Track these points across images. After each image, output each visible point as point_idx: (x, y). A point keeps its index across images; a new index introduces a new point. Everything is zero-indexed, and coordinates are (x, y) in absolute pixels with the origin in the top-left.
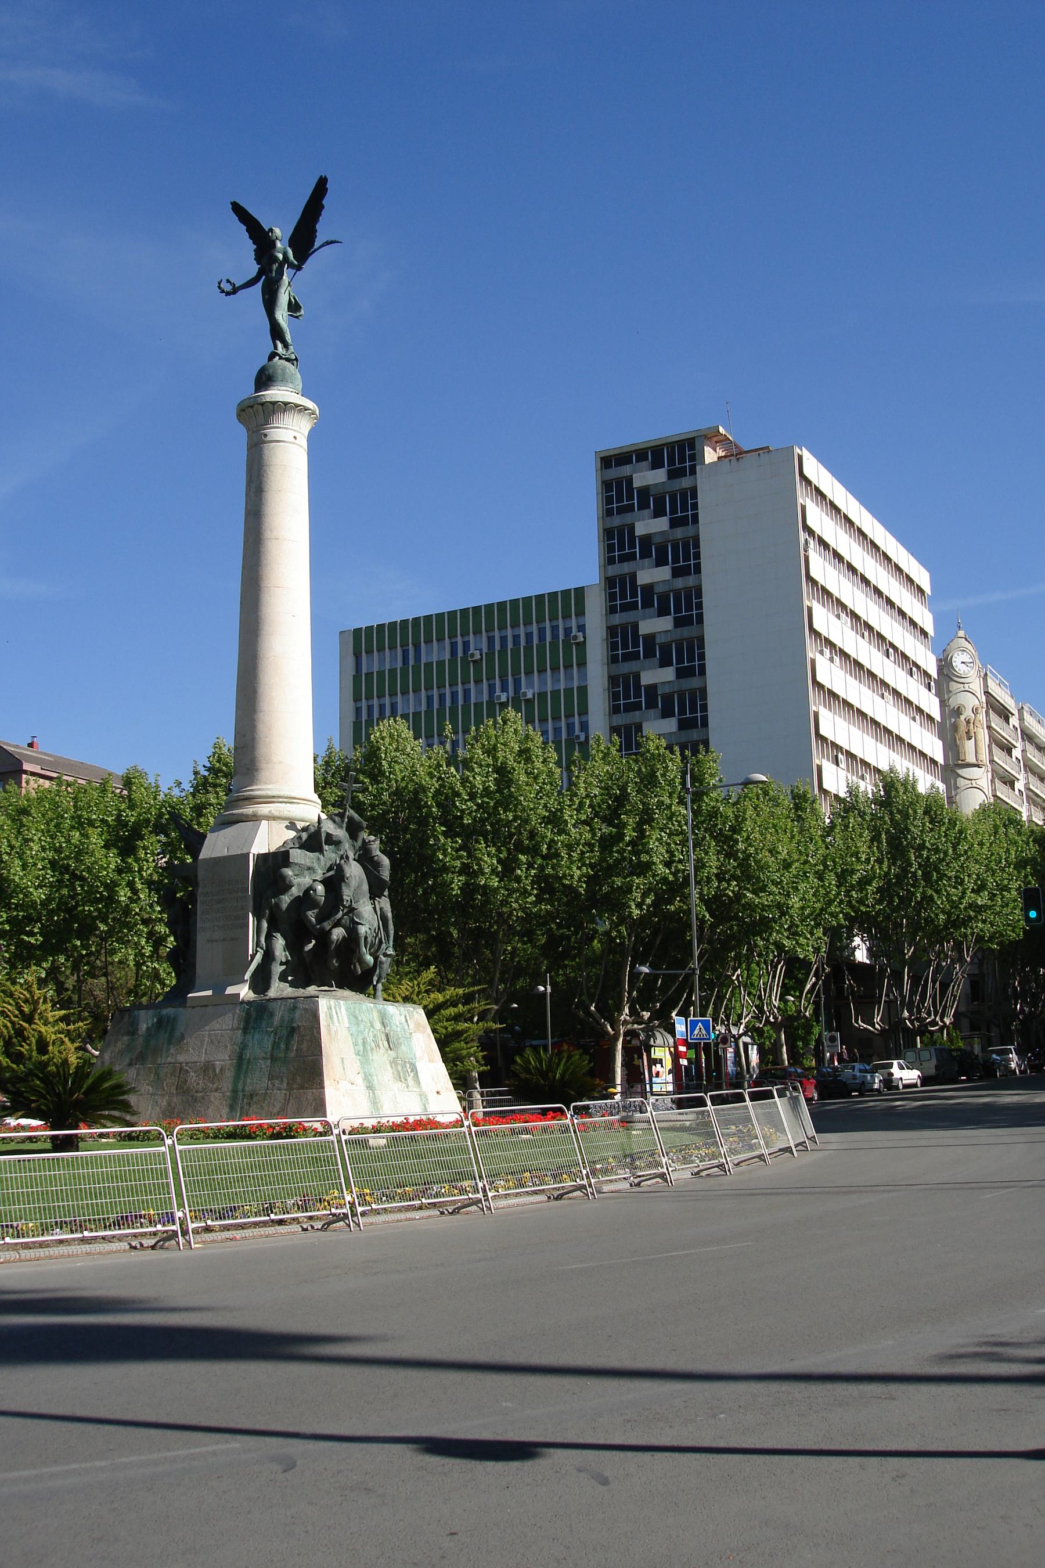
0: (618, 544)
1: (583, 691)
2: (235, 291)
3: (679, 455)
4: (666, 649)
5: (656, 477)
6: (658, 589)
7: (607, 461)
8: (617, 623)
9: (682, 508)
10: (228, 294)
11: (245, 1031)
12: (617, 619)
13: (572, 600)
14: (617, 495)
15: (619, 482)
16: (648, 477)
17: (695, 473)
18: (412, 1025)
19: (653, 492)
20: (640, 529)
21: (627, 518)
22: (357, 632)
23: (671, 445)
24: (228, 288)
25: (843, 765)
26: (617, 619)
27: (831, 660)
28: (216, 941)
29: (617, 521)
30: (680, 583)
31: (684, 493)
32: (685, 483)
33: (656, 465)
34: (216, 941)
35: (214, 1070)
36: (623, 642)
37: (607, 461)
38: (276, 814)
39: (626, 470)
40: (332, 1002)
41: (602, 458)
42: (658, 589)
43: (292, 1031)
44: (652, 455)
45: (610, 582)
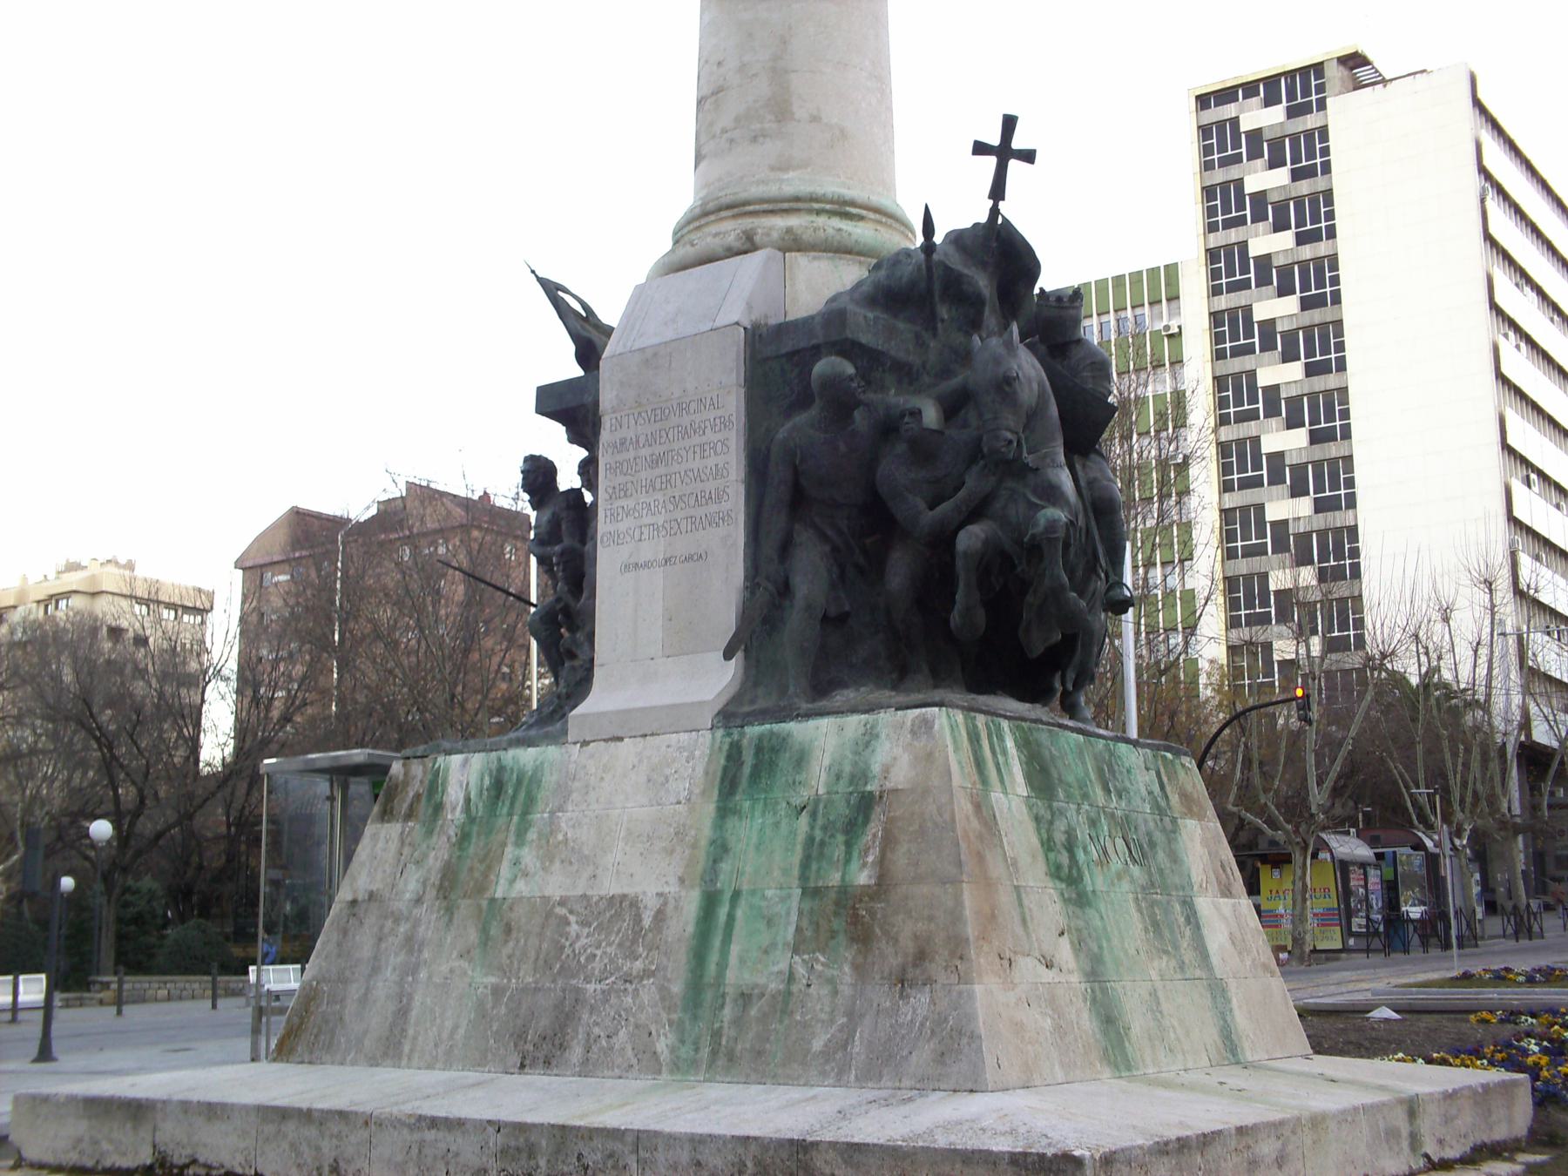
0: (1224, 204)
1: (1179, 398)
3: (1300, 87)
4: (1290, 337)
5: (1273, 117)
6: (1278, 261)
7: (1203, 101)
8: (1224, 307)
9: (1308, 154)
11: (725, 811)
13: (1162, 285)
14: (1220, 141)
15: (1221, 125)
16: (1257, 117)
18: (1175, 799)
19: (1267, 135)
20: (1251, 186)
21: (1234, 172)
23: (1290, 74)
25: (1536, 488)
26: (1223, 302)
27: (1518, 347)
28: (646, 565)
30: (1307, 252)
31: (1309, 134)
32: (1311, 121)
33: (1270, 101)
34: (646, 565)
35: (638, 919)
36: (1231, 330)
37: (1203, 101)
38: (807, 236)
39: (1229, 111)
40: (981, 720)
41: (1198, 97)
42: (1278, 261)
43: (865, 804)
44: (1268, 88)
45: (1212, 255)
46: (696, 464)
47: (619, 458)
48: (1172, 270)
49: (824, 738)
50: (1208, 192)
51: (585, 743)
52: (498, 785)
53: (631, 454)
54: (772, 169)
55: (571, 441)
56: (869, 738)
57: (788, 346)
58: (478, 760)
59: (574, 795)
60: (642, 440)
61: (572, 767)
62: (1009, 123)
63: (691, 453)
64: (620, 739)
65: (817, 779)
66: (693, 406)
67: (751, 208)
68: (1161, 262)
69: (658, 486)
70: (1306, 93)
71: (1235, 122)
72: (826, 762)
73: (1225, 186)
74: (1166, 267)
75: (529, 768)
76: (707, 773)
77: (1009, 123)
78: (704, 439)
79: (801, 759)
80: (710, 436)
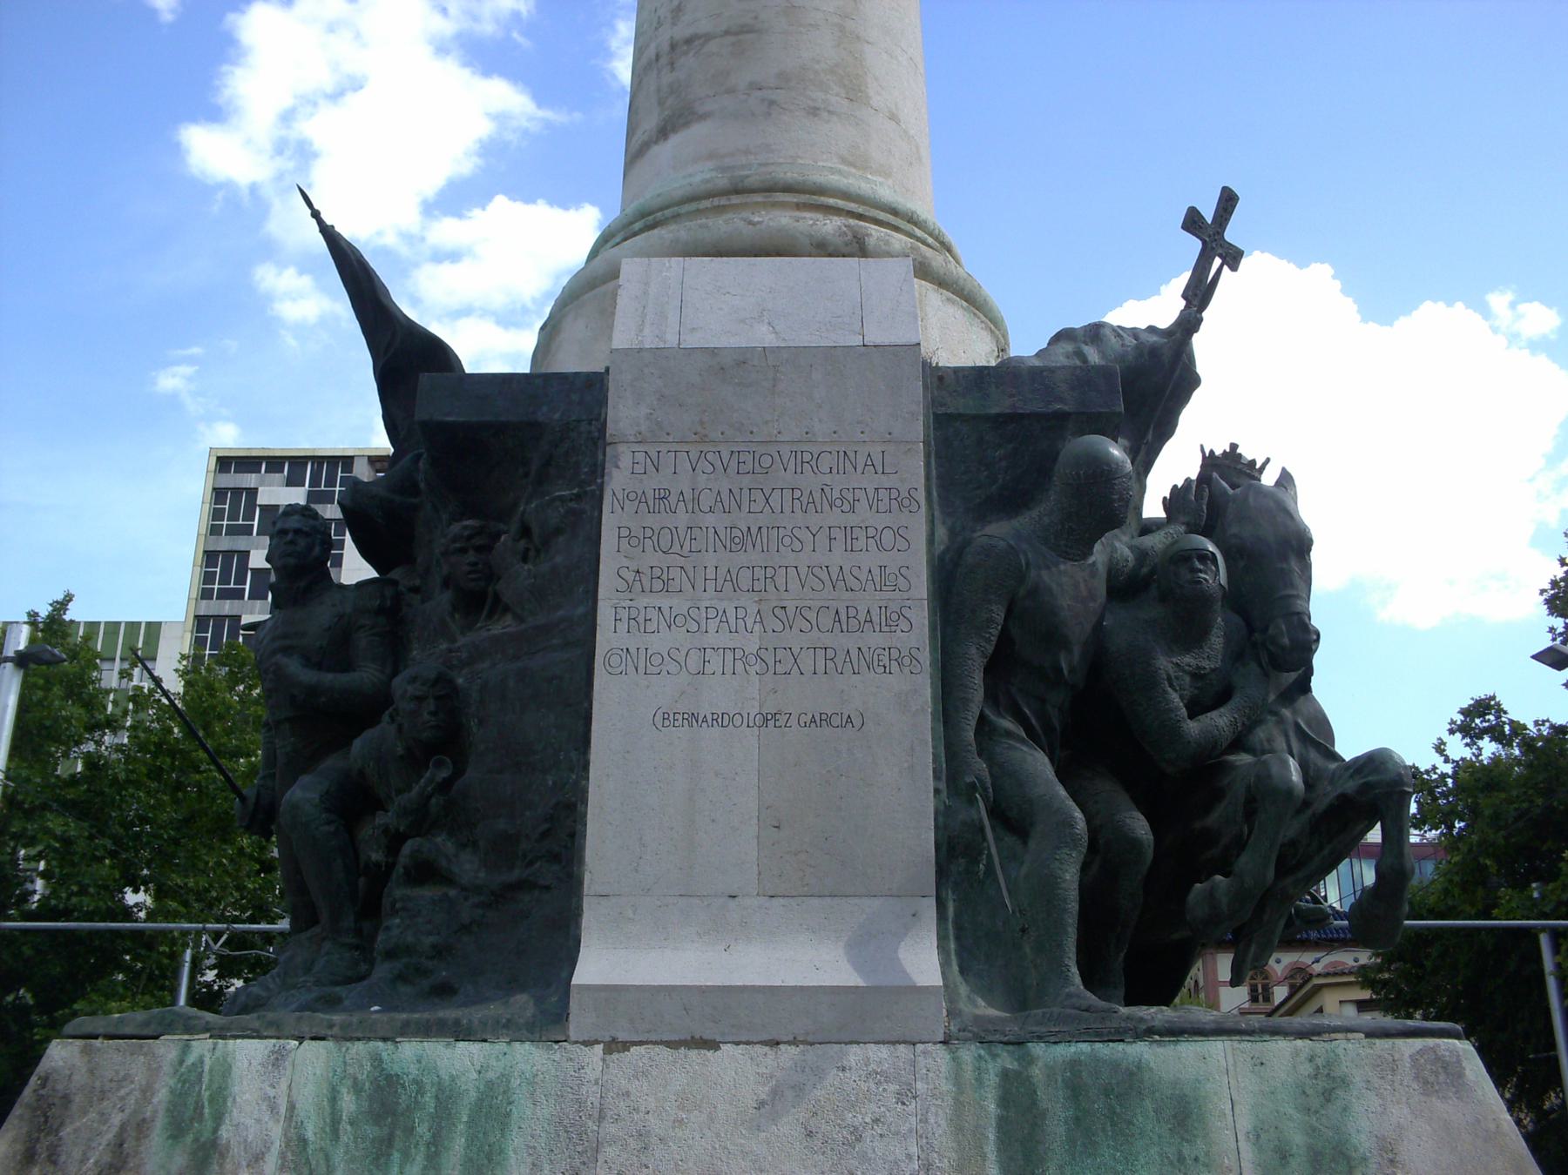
7: (224, 463)
15: (237, 492)
21: (240, 543)
28: (717, 719)
39: (249, 480)
41: (219, 458)
45: (201, 622)
46: (837, 557)
47: (650, 520)
48: (154, 629)
50: (210, 557)
51: (615, 1046)
52: (387, 1103)
53: (682, 519)
54: (844, 161)
55: (1193, 382)
57: (1000, 404)
58: (313, 1061)
59: (610, 1152)
60: (707, 500)
61: (591, 1095)
62: (1228, 201)
63: (822, 538)
64: (713, 1045)
66: (826, 462)
67: (831, 201)
68: (143, 616)
69: (745, 583)
70: (331, 482)
71: (252, 492)
72: (1245, 1123)
73: (228, 554)
74: (149, 624)
75: (470, 1084)
76: (957, 1126)
77: (1228, 201)
78: (852, 520)
79: (1184, 1114)
80: (863, 514)
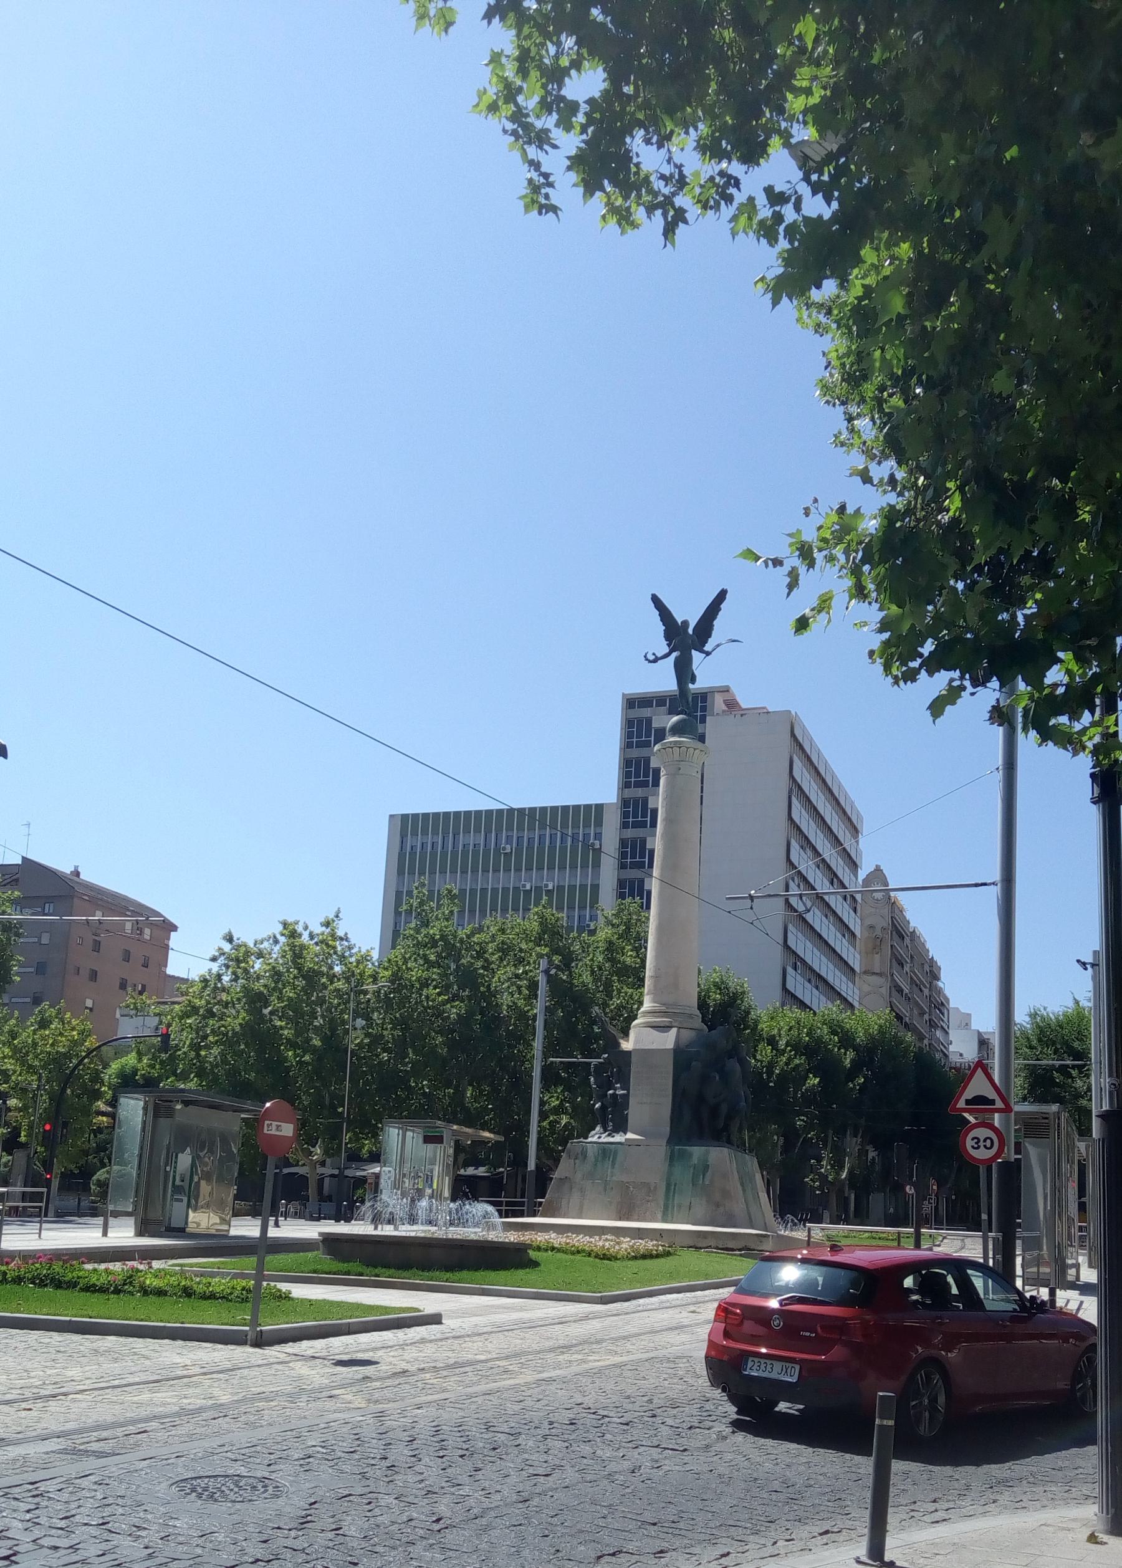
1: (596, 888)
2: (655, 661)
7: (632, 703)
10: (650, 662)
12: (630, 833)
17: (705, 722)
22: (405, 817)
24: (652, 658)
26: (630, 833)
29: (635, 753)
37: (632, 703)
39: (646, 712)
45: (625, 802)
48: (599, 807)
49: (697, 1152)
56: (707, 1153)
65: (695, 1160)
79: (691, 1155)
